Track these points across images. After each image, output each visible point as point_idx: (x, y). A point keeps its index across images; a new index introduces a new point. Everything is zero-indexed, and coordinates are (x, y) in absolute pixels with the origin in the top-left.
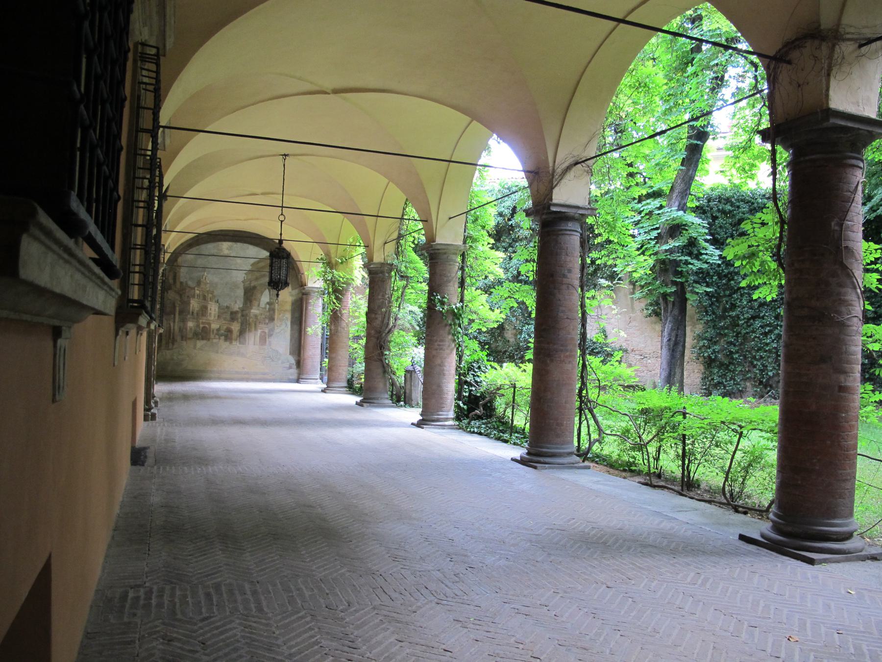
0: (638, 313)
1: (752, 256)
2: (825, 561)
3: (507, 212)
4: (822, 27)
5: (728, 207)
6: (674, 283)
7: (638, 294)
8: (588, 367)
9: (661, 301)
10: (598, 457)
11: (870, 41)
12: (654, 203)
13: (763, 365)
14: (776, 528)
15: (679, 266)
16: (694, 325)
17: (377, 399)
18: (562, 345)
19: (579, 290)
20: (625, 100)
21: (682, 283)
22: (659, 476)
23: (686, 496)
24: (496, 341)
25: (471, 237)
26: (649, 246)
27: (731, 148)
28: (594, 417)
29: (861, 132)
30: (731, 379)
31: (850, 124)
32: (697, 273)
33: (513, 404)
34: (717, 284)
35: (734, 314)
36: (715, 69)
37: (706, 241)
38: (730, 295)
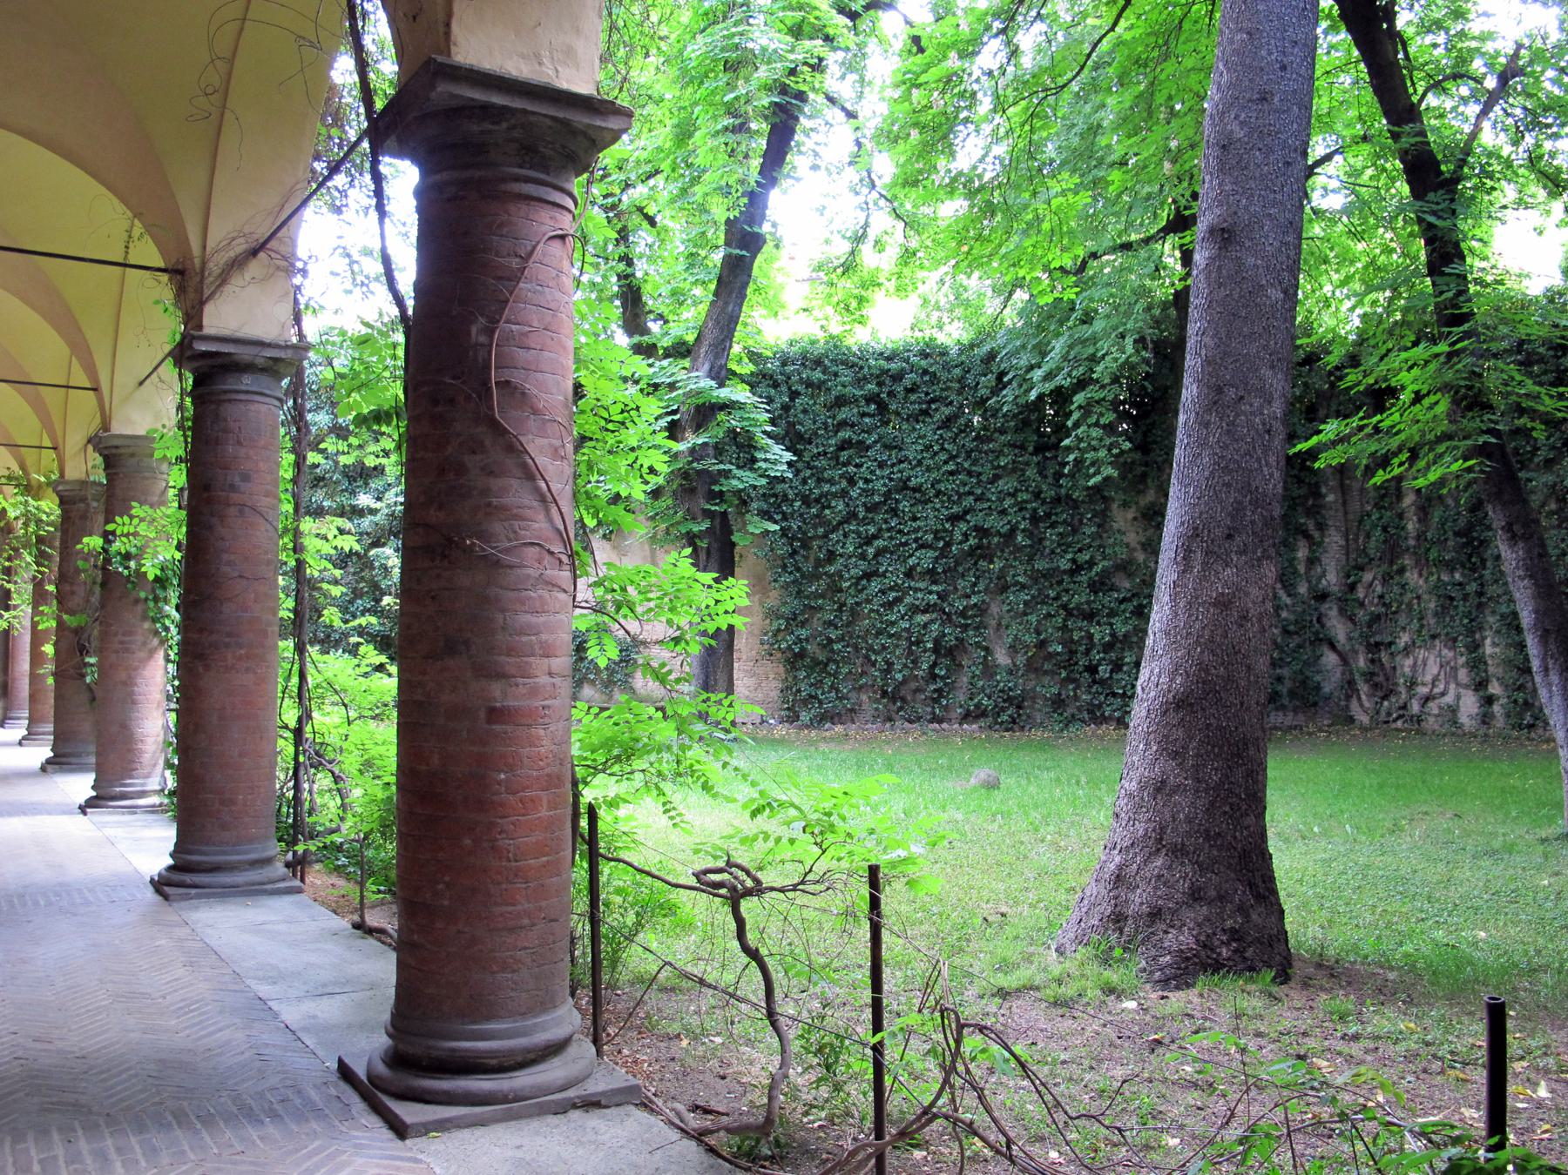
2: (443, 1126)
5: (818, 375)
6: (708, 514)
17: (79, 755)
18: (229, 635)
29: (532, 118)
30: (832, 687)
31: (498, 99)
34: (801, 515)
37: (768, 435)
38: (825, 536)
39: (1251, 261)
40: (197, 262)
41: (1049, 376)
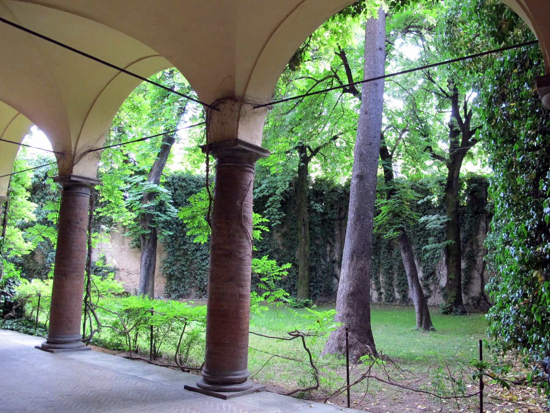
0: (127, 246)
1: (194, 217)
2: (232, 396)
3: (42, 175)
4: (236, 94)
5: (184, 184)
6: (150, 228)
7: (127, 234)
8: (92, 282)
9: (141, 239)
10: (97, 341)
11: (259, 106)
12: (140, 178)
13: (201, 279)
14: (206, 380)
15: (153, 217)
16: (161, 254)
19: (88, 232)
20: (125, 115)
21: (155, 228)
22: (136, 352)
23: (153, 364)
24: (28, 262)
25: (13, 192)
26: (135, 204)
27: (187, 149)
28: (94, 315)
30: (183, 287)
31: (248, 149)
32: (164, 222)
33: (38, 308)
35: (185, 247)
36: (181, 102)
37: (170, 203)
39: (367, 184)
40: (73, 153)
41: (261, 191)
